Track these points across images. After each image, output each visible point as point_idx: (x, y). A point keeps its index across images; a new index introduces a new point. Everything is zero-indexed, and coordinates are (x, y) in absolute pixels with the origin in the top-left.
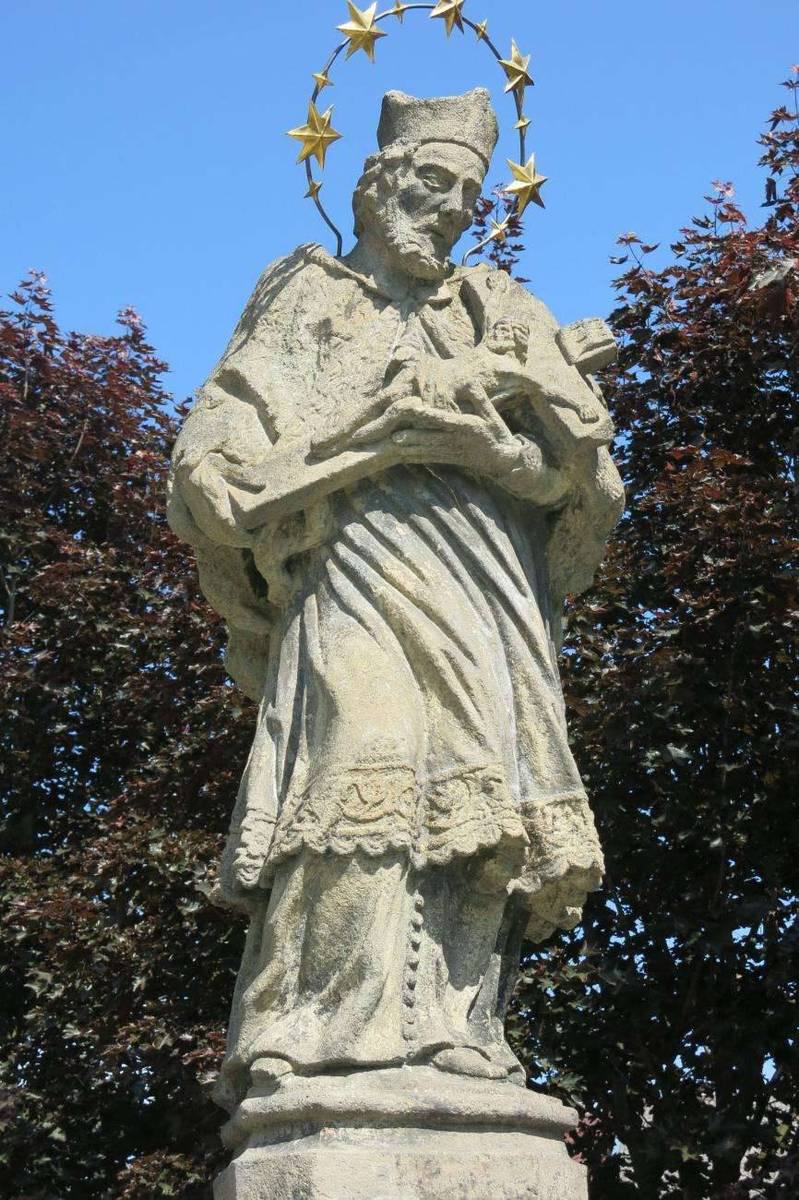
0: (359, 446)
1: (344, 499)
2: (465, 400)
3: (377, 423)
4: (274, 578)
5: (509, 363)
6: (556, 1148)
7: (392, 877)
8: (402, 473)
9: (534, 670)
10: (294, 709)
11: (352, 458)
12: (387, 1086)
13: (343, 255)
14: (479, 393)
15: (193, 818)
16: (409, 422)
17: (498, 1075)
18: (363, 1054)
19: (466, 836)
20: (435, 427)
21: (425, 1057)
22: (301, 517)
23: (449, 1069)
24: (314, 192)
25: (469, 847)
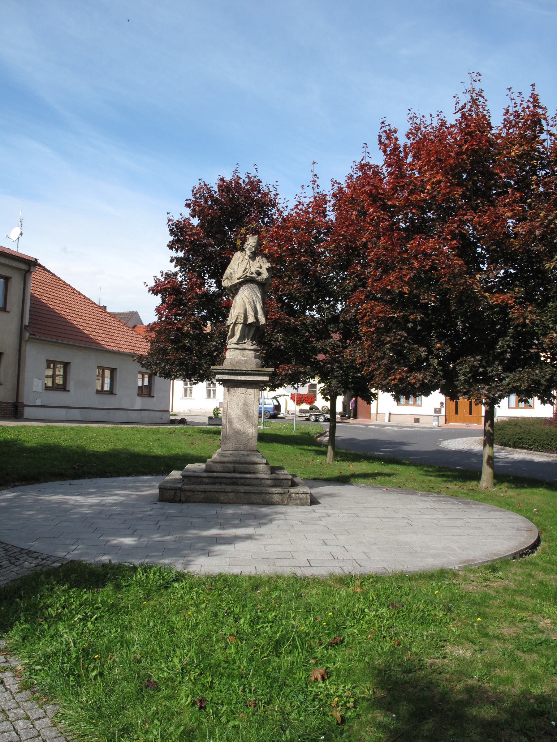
2: (252, 273)
4: (234, 292)
11: (241, 280)
16: (247, 276)
20: (249, 277)
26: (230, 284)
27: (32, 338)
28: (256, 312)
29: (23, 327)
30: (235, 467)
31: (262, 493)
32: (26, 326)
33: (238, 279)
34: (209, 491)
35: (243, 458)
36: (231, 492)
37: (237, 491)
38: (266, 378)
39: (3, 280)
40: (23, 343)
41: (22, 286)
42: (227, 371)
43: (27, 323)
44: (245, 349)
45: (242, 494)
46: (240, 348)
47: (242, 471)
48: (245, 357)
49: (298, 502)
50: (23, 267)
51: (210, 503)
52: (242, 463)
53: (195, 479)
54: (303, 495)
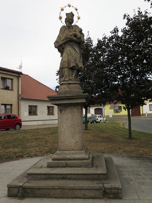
0: (65, 40)
1: (64, 44)
3: (65, 38)
4: (62, 50)
5: (74, 33)
6: (79, 85)
7: (66, 69)
8: (68, 41)
9: (78, 54)
10: (129, 125)
11: (64, 41)
12: (67, 82)
13: (106, 190)
14: (72, 35)
15: (144, 98)
16: (67, 38)
17: (81, 149)
18: (65, 80)
19: (71, 66)
21: (70, 80)
22: (62, 46)
23: (71, 81)
24: (61, 22)
25: (71, 67)
26: (58, 45)
27: (22, 99)
28: (75, 60)
29: (19, 95)
30: (66, 163)
31: (82, 189)
32: (20, 95)
33: (62, 41)
34: (42, 189)
35: (72, 155)
36: (58, 189)
37: (63, 188)
38: (84, 101)
39: (11, 80)
40: (19, 101)
41: (17, 81)
42: (58, 98)
43: (20, 94)
44: (70, 84)
45: (67, 190)
46: (67, 83)
47: (71, 165)
48: (69, 89)
49: (112, 196)
50: (17, 75)
51: (43, 197)
52: (72, 160)
53: (36, 176)
54: (116, 190)
